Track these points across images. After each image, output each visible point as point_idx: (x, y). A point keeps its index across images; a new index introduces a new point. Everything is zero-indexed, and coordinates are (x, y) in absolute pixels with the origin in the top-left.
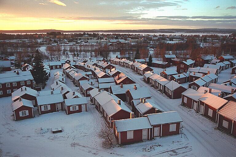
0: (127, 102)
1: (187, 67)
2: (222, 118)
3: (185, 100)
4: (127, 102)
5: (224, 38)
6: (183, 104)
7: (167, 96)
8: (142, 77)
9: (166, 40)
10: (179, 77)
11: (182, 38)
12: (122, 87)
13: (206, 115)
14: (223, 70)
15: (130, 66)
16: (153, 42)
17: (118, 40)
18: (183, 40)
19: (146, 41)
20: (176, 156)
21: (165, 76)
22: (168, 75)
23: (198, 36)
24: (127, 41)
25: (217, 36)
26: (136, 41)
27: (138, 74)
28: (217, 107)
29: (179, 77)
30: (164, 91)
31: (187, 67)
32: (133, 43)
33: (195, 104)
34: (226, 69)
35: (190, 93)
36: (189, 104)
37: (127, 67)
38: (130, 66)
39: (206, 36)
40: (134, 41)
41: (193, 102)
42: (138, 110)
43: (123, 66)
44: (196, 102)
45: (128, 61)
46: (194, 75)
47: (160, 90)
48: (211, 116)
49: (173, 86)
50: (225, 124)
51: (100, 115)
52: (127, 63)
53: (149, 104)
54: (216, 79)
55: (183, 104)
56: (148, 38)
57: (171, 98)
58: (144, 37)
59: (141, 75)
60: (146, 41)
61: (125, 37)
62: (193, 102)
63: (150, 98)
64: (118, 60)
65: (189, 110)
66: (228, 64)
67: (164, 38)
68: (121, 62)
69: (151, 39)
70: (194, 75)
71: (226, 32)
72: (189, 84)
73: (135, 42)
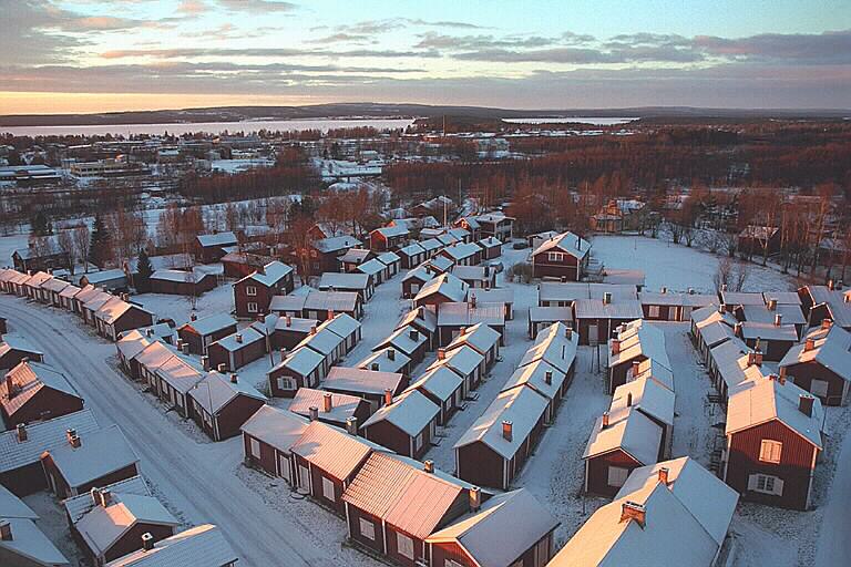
0: (52, 491)
1: (265, 296)
2: (358, 514)
3: (256, 452)
4: (52, 491)
5: (392, 143)
6: (251, 462)
7: (201, 427)
8: (111, 349)
9: (208, 158)
10: (241, 342)
11: (261, 142)
12: (23, 437)
13: (317, 496)
14: (380, 282)
15: (68, 303)
16: (159, 169)
17: (21, 168)
18: (266, 152)
19: (136, 166)
20: (377, 17)
21: (191, 342)
22: (205, 336)
23: (313, 135)
24: (58, 170)
25: (372, 133)
26: (96, 169)
27: (101, 334)
28: (342, 476)
29: (241, 342)
30: (188, 410)
31: (265, 296)
32: (84, 176)
33: (285, 462)
34: (389, 277)
35: (268, 424)
36: (265, 460)
37: (56, 305)
38: (68, 303)
39: (340, 133)
40: (90, 170)
41: (278, 458)
42: (85, 537)
43: (42, 301)
44: (285, 455)
45: (57, 285)
46: (288, 326)
47: (176, 408)
48: (332, 498)
49: (217, 391)
50: (367, 529)
51: (76, 320)
52: (54, 292)
53: (125, 508)
54: (357, 332)
55: (251, 462)
56: (141, 152)
57: (213, 439)
58: (125, 149)
59: (110, 338)
60: (136, 166)
61: (53, 150)
62: (278, 458)
63: (129, 472)
64: (20, 278)
65: (269, 482)
66: (394, 263)
67: (198, 148)
68: (32, 288)
69: (151, 157)
70: (288, 326)
71: (397, 114)
72: (271, 374)
73: (87, 173)
